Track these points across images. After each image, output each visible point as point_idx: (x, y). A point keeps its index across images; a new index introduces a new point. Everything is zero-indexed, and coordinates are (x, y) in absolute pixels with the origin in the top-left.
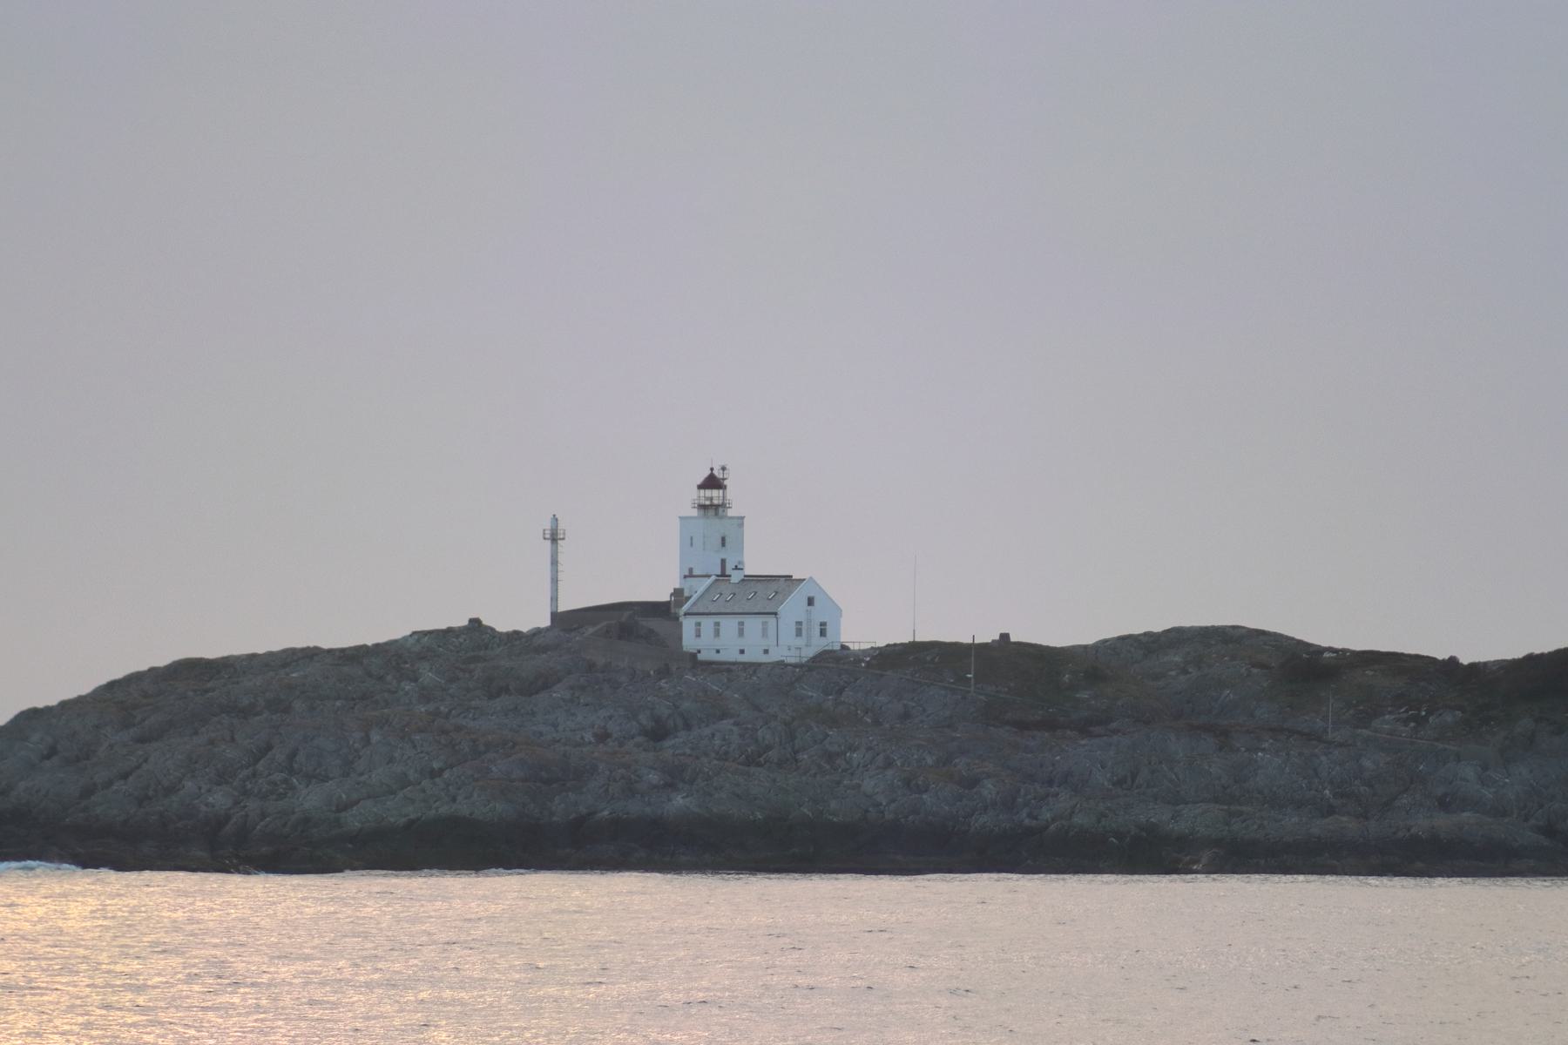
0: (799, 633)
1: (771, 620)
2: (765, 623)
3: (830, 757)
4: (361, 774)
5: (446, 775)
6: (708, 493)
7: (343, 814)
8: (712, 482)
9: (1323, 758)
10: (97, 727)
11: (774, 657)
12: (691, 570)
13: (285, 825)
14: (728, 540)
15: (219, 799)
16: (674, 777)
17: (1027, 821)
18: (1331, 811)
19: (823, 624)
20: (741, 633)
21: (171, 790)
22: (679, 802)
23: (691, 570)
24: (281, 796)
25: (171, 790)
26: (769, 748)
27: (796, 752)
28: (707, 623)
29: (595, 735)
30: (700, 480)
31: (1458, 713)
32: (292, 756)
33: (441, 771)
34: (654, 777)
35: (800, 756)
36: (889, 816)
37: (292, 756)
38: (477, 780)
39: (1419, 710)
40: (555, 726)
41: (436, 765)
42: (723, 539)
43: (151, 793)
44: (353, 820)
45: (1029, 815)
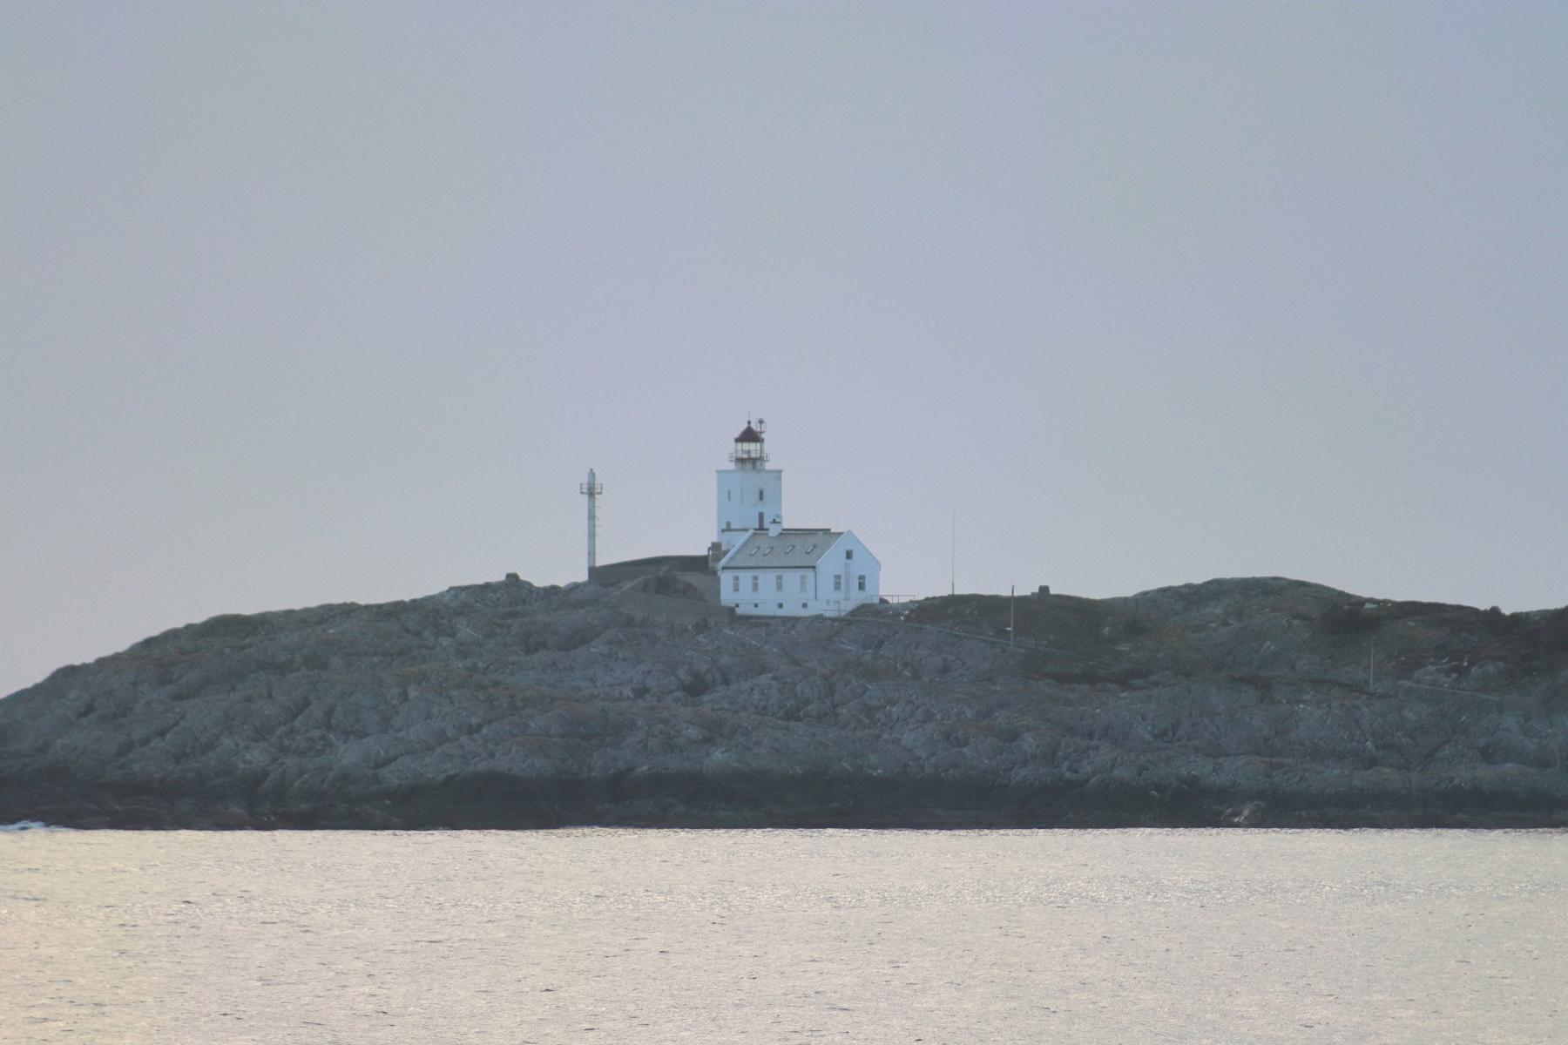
0: (837, 586)
1: (810, 574)
3: (870, 711)
6: (746, 446)
7: (381, 771)
8: (749, 436)
10: (134, 684)
12: (728, 524)
15: (257, 756)
16: (714, 732)
17: (1068, 775)
18: (1373, 763)
19: (862, 578)
20: (779, 587)
22: (718, 757)
23: (728, 524)
25: (209, 747)
26: (808, 702)
28: (745, 577)
30: (737, 434)
32: (330, 712)
33: (480, 727)
34: (692, 732)
36: (929, 770)
37: (330, 712)
39: (1462, 660)
40: (593, 680)
41: (474, 721)
42: (761, 493)
43: (188, 750)
44: (392, 777)
45: (1070, 769)
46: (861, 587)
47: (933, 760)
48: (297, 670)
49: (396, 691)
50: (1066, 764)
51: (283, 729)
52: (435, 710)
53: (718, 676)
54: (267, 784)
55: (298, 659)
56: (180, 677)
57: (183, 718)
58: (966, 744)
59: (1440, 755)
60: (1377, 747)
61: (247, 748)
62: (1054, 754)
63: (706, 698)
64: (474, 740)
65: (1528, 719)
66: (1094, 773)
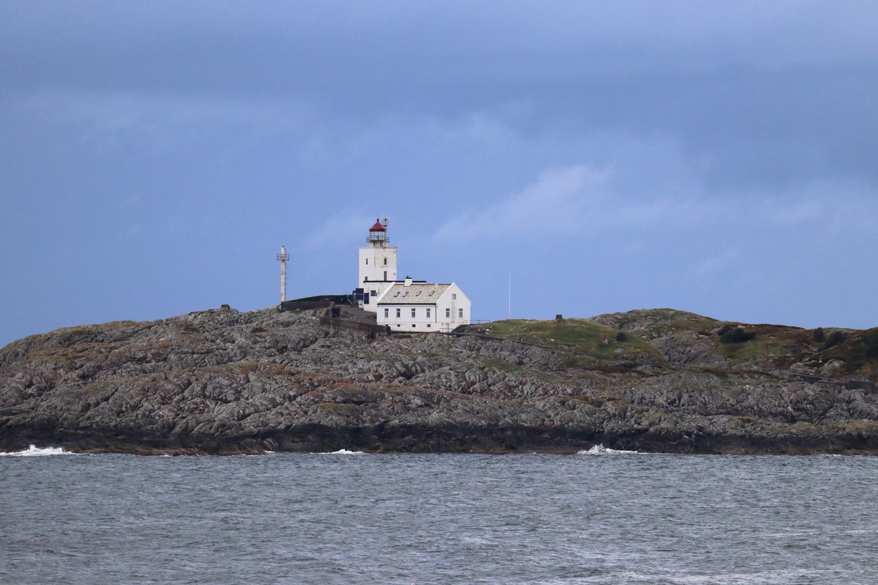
0: (448, 315)
1: (432, 308)
2: (428, 310)
3: (510, 388)
4: (247, 399)
5: (298, 399)
6: (376, 233)
7: (242, 422)
8: (378, 228)
9: (784, 389)
10: (55, 369)
11: (434, 329)
12: (366, 278)
13: (211, 428)
14: (383, 262)
15: (166, 413)
16: (429, 402)
17: (636, 426)
18: (793, 420)
19: (461, 310)
20: (414, 315)
21: (135, 408)
22: (434, 416)
23: (366, 278)
24: (202, 412)
25: (135, 408)
26: (473, 383)
27: (490, 386)
28: (393, 310)
29: (374, 376)
30: (371, 227)
31: (842, 362)
32: (204, 387)
33: (295, 397)
34: (418, 401)
35: (492, 388)
36: (557, 423)
37: (204, 387)
38: (317, 402)
39: (818, 360)
40: (346, 369)
41: (292, 393)
42: (385, 260)
43: (124, 409)
44: (250, 425)
45: (636, 422)
46: (461, 315)
47: (558, 417)
48: (149, 362)
49: (242, 376)
50: (633, 421)
51: (178, 397)
52: (267, 387)
53: (419, 368)
54: (177, 429)
55: (149, 355)
56: (82, 366)
57: (116, 390)
58: (574, 408)
59: (828, 414)
60: (794, 409)
61: (159, 408)
62: (625, 413)
63: (414, 380)
64: (293, 405)
65: (866, 394)
66: (651, 425)
